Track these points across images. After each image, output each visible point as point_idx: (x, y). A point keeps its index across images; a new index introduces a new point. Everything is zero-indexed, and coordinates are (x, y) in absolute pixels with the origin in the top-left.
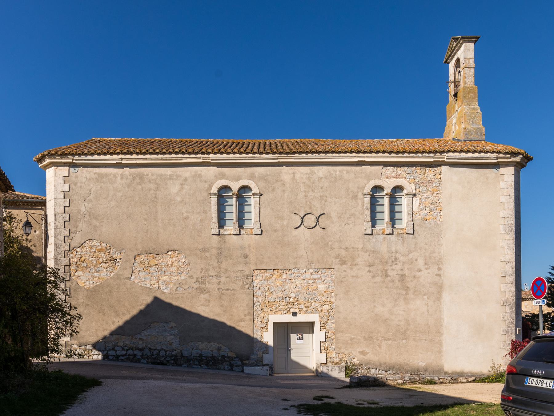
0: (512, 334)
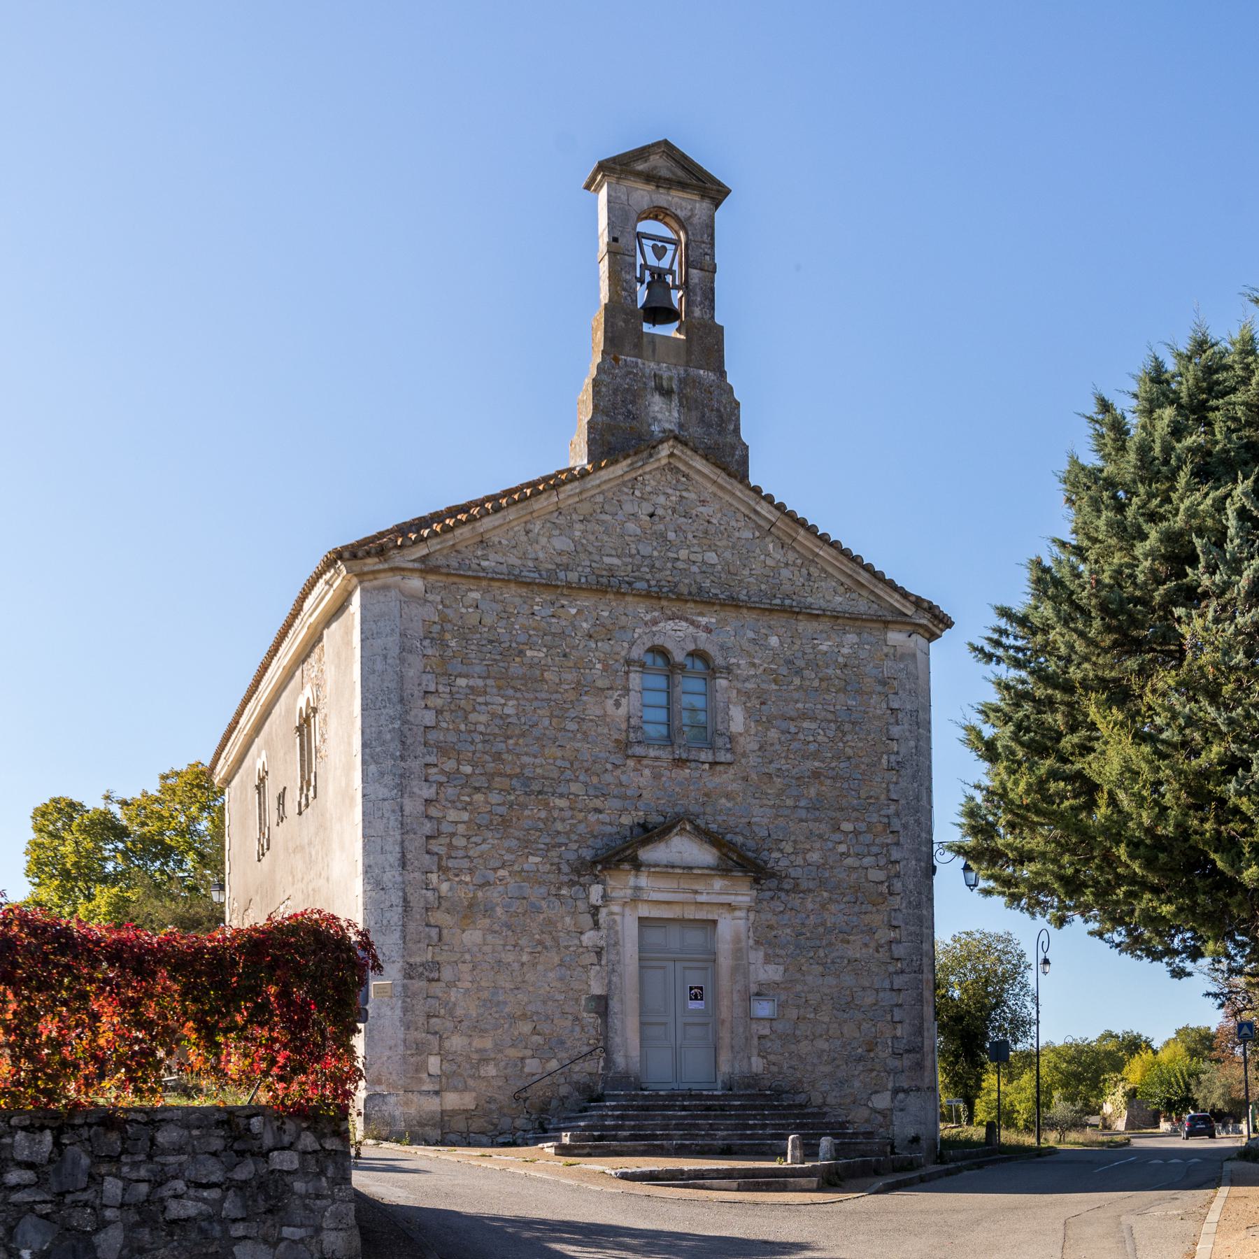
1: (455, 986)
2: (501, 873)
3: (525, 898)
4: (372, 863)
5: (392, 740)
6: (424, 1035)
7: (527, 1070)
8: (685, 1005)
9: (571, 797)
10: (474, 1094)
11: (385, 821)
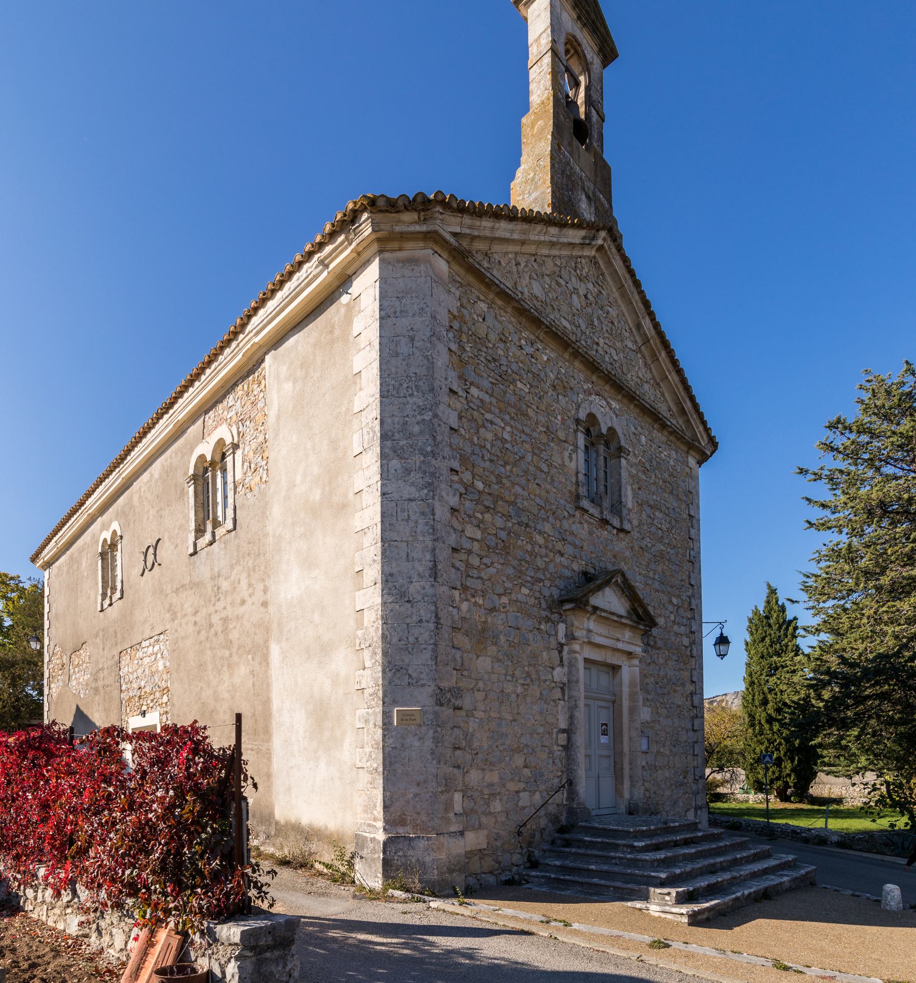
0: (375, 725)
1: (473, 716)
2: (505, 600)
3: (518, 629)
4: (394, 571)
5: (421, 432)
6: (451, 769)
7: (521, 804)
8: (599, 738)
9: (545, 535)
10: (486, 832)
11: (412, 524)
